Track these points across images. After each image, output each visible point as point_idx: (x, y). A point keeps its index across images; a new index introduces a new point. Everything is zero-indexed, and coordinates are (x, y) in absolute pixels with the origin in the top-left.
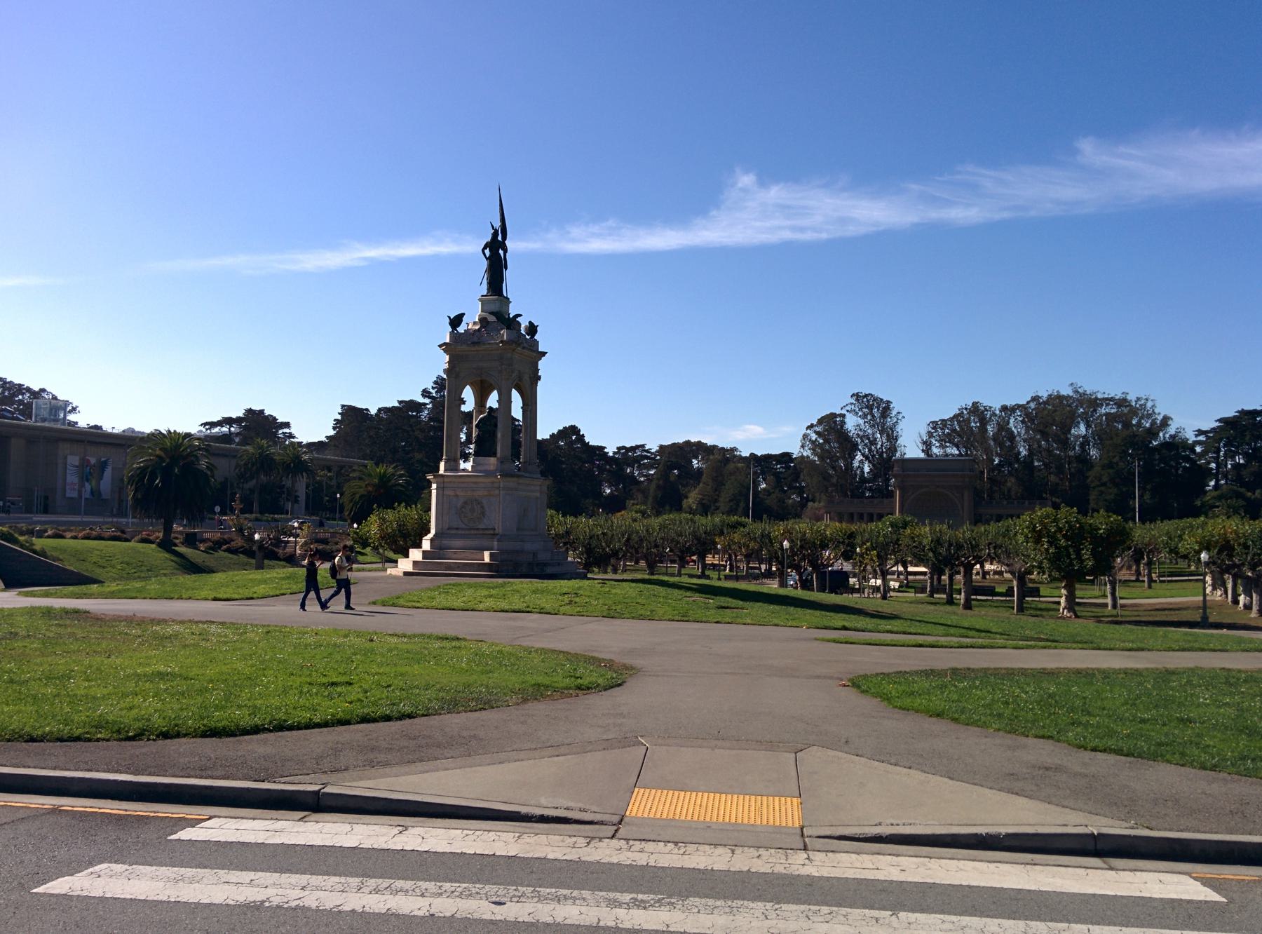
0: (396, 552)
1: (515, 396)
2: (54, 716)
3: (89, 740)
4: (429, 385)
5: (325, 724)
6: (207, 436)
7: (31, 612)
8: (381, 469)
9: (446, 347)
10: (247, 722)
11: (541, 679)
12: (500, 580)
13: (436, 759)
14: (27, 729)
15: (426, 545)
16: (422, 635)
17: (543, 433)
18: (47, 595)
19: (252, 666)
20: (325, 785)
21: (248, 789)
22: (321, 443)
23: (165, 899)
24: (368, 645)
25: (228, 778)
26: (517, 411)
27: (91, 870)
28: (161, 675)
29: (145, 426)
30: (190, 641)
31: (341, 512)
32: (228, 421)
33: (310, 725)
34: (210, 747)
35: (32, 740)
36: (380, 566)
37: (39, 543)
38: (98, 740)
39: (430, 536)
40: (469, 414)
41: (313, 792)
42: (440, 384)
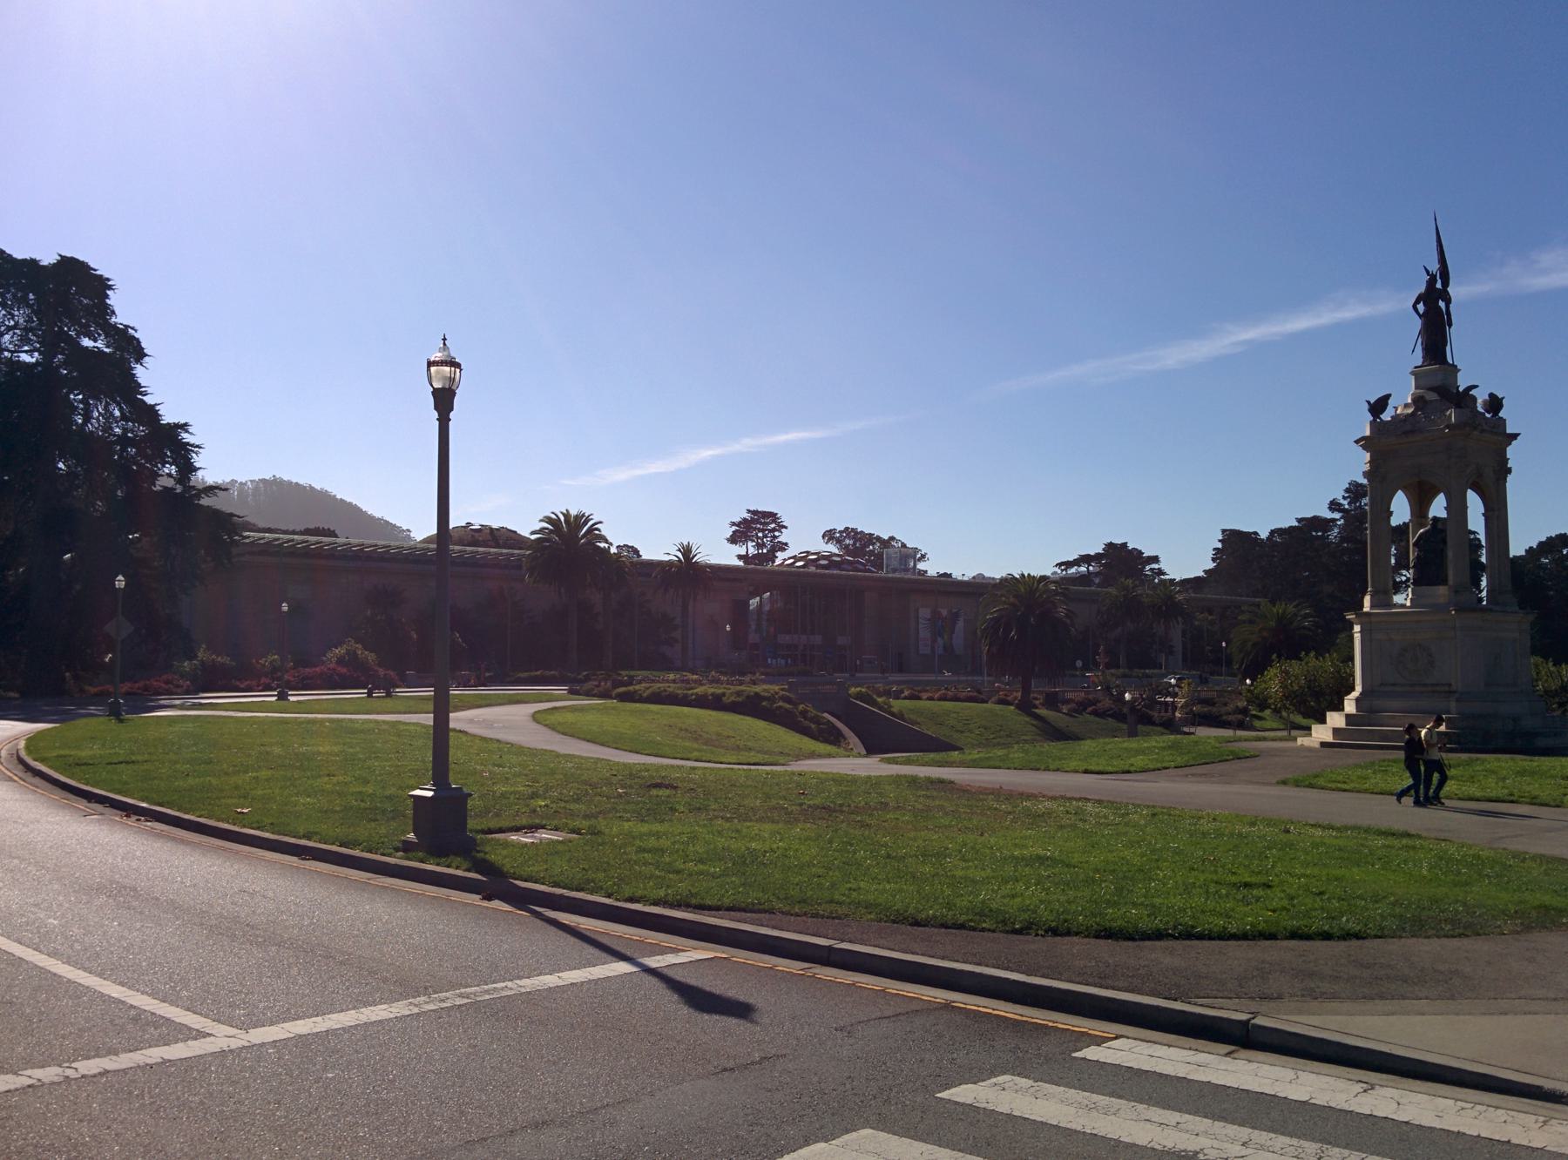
0: (1306, 715)
1: (1475, 506)
2: (936, 899)
3: (974, 929)
4: (1339, 494)
5: (1244, 937)
6: (1063, 579)
7: (897, 780)
8: (1278, 609)
9: (1365, 443)
10: (1145, 924)
11: (1547, 899)
12: (1464, 756)
13: (1404, 998)
14: (911, 910)
15: (1350, 706)
16: (1355, 828)
17: (1517, 548)
18: (908, 762)
19: (1142, 855)
20: (1255, 1014)
21: (1157, 1007)
22: (1197, 579)
23: (1079, 1128)
24: (1283, 837)
25: (1132, 991)
26: (1476, 521)
27: (994, 1080)
28: (1041, 859)
29: (996, 572)
30: (1065, 822)
31: (1229, 663)
32: (1085, 559)
33: (1224, 936)
34: (1104, 947)
35: (917, 923)
36: (1285, 733)
37: (897, 705)
38: (983, 930)
39: (1355, 694)
40: (1402, 530)
41: (1240, 1022)
42: (1355, 491)
